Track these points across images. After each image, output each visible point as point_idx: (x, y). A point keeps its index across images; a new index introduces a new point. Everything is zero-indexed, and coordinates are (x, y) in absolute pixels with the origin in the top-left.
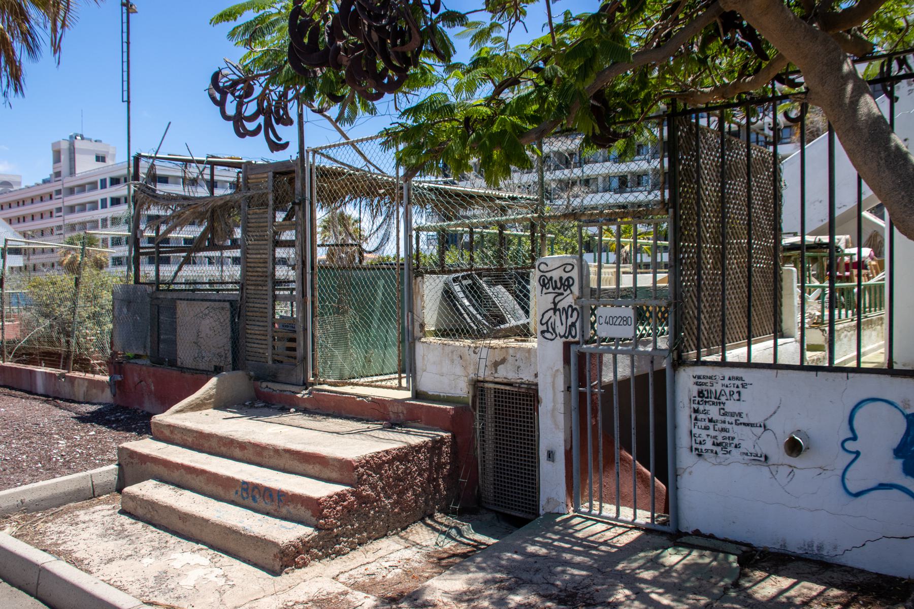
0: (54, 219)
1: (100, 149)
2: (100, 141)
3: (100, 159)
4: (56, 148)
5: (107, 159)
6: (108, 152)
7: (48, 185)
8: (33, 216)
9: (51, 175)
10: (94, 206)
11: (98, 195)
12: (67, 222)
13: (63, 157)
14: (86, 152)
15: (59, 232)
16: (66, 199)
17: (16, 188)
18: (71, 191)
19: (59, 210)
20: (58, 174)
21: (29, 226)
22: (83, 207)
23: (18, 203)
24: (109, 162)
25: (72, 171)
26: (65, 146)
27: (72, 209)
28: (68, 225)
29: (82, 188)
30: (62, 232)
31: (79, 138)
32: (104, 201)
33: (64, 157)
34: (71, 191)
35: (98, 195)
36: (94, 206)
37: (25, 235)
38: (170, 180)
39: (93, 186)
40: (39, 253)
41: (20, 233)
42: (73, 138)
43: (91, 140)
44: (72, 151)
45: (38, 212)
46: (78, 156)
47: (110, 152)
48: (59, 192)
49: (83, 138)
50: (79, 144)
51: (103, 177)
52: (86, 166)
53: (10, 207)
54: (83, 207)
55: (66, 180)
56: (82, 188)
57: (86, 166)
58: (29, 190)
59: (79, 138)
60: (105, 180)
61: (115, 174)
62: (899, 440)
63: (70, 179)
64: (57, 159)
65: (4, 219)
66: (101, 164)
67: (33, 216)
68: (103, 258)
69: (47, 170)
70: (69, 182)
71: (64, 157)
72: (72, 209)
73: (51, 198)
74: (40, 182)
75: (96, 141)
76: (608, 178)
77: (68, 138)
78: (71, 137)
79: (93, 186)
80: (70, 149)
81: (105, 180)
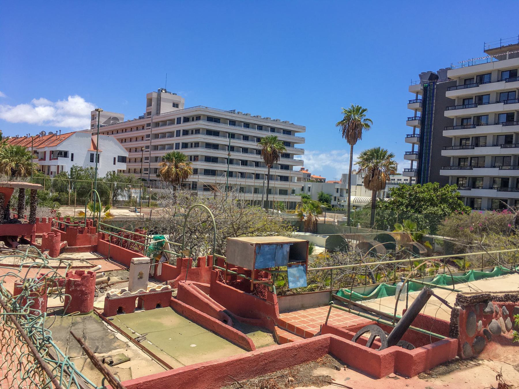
0: (144, 142)
1: (176, 99)
2: (176, 94)
3: (175, 105)
4: (149, 97)
5: (179, 106)
6: (180, 101)
7: (142, 120)
8: (137, 138)
9: (144, 114)
10: (171, 135)
11: (174, 128)
12: (152, 144)
13: (153, 103)
14: (167, 101)
15: (147, 150)
16: (153, 129)
17: (120, 121)
18: (157, 125)
19: (148, 136)
20: (149, 114)
21: (134, 144)
22: (164, 135)
23: (123, 130)
24: (180, 108)
25: (158, 112)
26: (155, 95)
27: (156, 136)
28: (153, 146)
29: (164, 123)
30: (149, 150)
31: (163, 91)
32: (178, 132)
33: (154, 103)
34: (157, 125)
35: (174, 128)
36: (171, 135)
37: (130, 150)
38: (221, 121)
39: (172, 122)
40: (133, 162)
41: (126, 149)
42: (160, 91)
43: (170, 93)
44: (159, 100)
45: (140, 136)
46: (162, 103)
47: (181, 102)
48: (149, 125)
49: (166, 92)
50: (163, 95)
51: (179, 116)
52: (166, 109)
53: (117, 133)
54: (164, 135)
55: (154, 118)
56: (164, 123)
57: (166, 109)
58: (129, 123)
59: (163, 91)
60: (180, 118)
61: (186, 115)
62: (147, 375)
63: (157, 117)
64: (149, 104)
65: (118, 139)
66: (176, 109)
67: (137, 138)
68: (189, 170)
69: (142, 111)
70: (156, 119)
71: (154, 103)
72: (156, 136)
73: (143, 129)
74: (138, 118)
75: (173, 94)
76: (498, 115)
77: (157, 91)
78: (159, 90)
79: (172, 122)
80: (158, 98)
81: (180, 118)
